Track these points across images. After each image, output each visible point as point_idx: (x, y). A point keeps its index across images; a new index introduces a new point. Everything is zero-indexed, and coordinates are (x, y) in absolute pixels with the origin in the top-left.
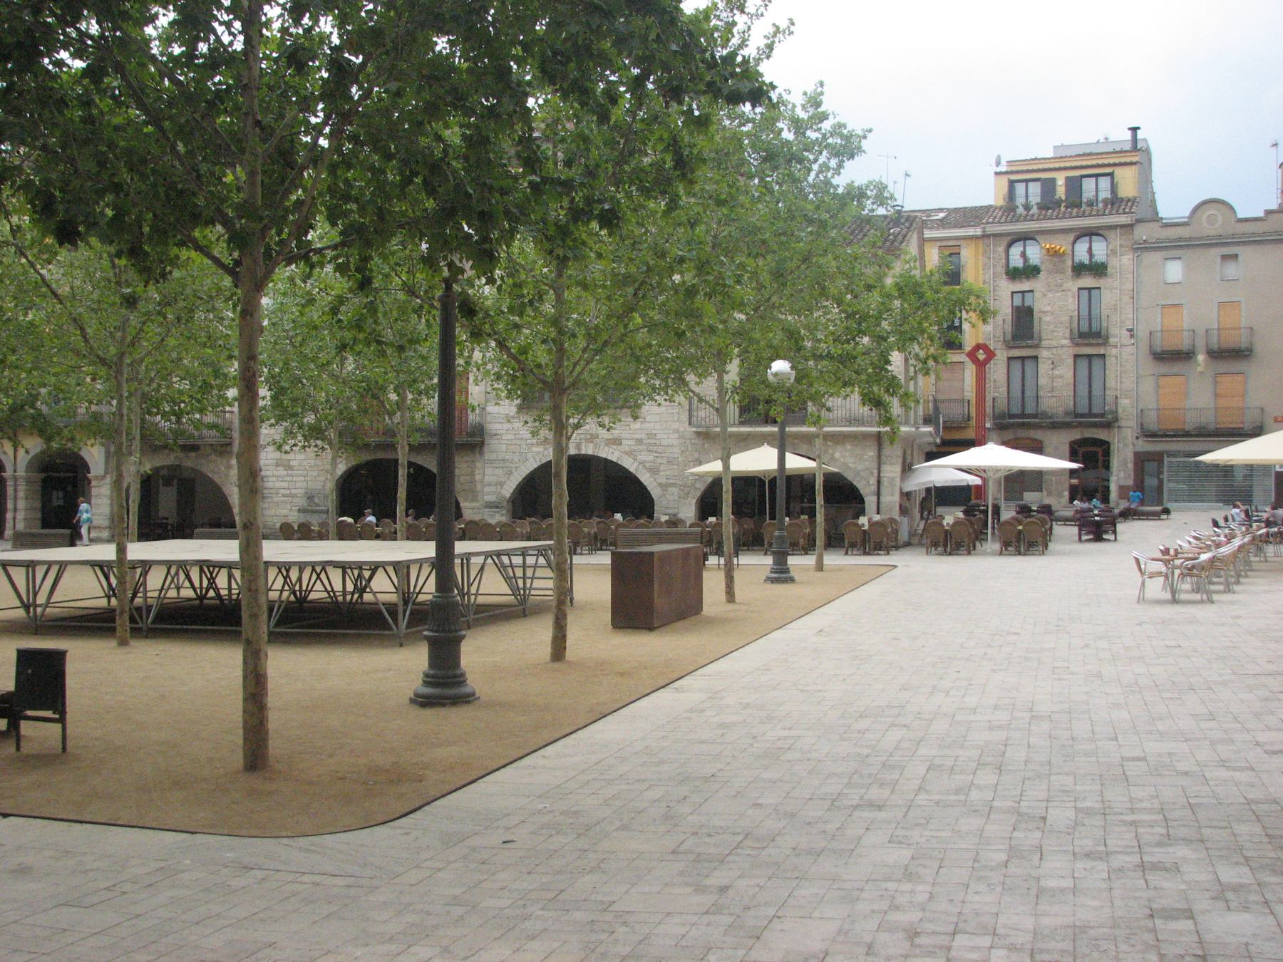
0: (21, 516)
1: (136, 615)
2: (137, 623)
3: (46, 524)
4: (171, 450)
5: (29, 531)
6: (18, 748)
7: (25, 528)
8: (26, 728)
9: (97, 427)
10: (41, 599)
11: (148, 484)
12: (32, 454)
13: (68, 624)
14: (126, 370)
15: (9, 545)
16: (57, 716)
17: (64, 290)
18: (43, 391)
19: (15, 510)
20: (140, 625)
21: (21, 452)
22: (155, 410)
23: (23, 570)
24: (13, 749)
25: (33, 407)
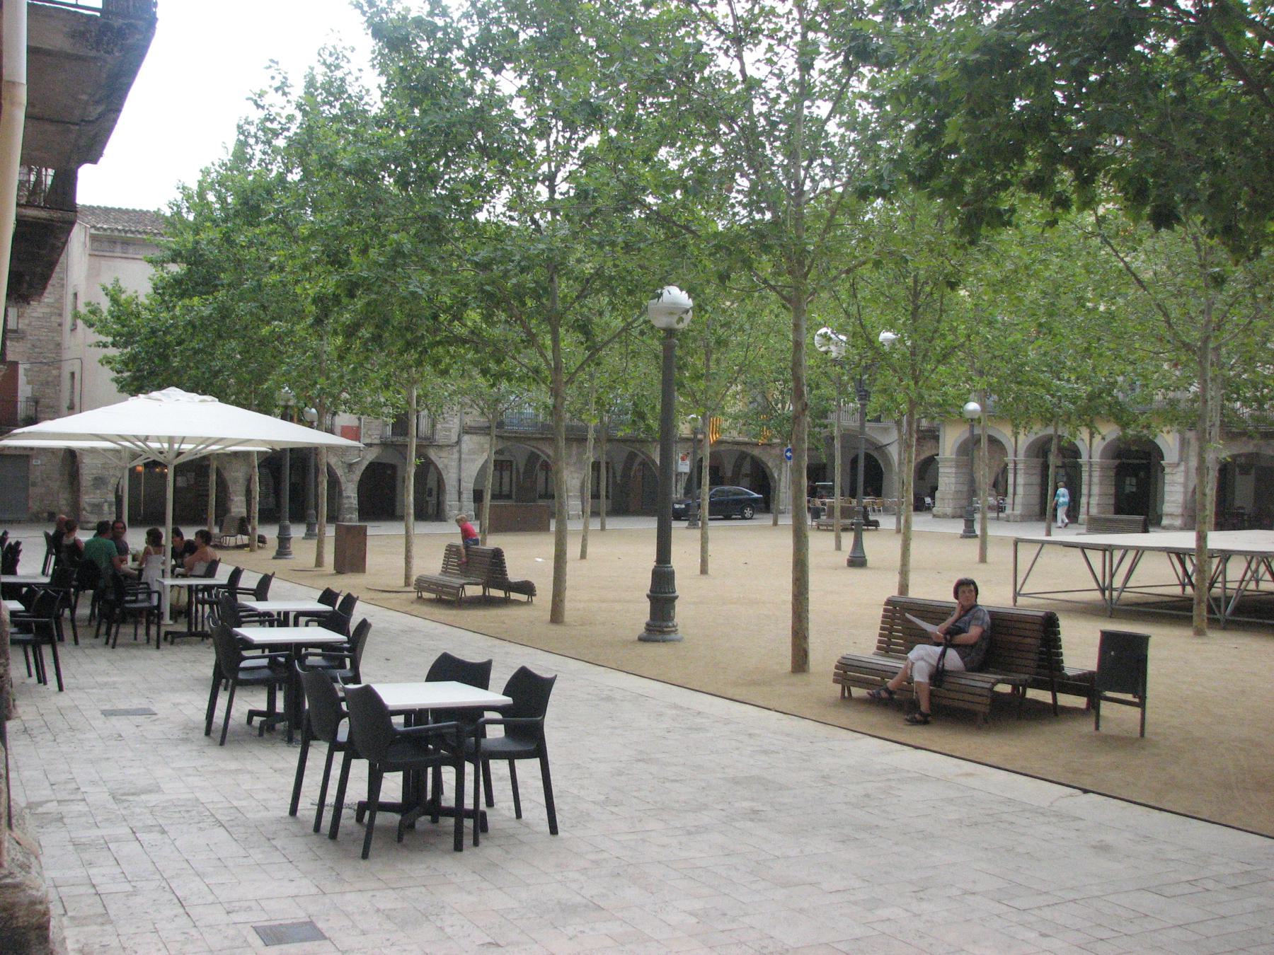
0: (1094, 501)
1: (1215, 605)
2: (1214, 614)
3: (1119, 510)
4: (1251, 437)
5: (1103, 516)
6: (1097, 728)
7: (1099, 513)
8: (1106, 708)
9: (1171, 414)
10: (1117, 583)
11: (1226, 472)
12: (1107, 441)
13: (1141, 609)
14: (1211, 356)
15: (1083, 529)
16: (1137, 700)
17: (1147, 276)
18: (1120, 379)
19: (1090, 496)
20: (1218, 616)
21: (1097, 438)
22: (1235, 396)
23: (1100, 553)
24: (1093, 727)
25: (1109, 394)
